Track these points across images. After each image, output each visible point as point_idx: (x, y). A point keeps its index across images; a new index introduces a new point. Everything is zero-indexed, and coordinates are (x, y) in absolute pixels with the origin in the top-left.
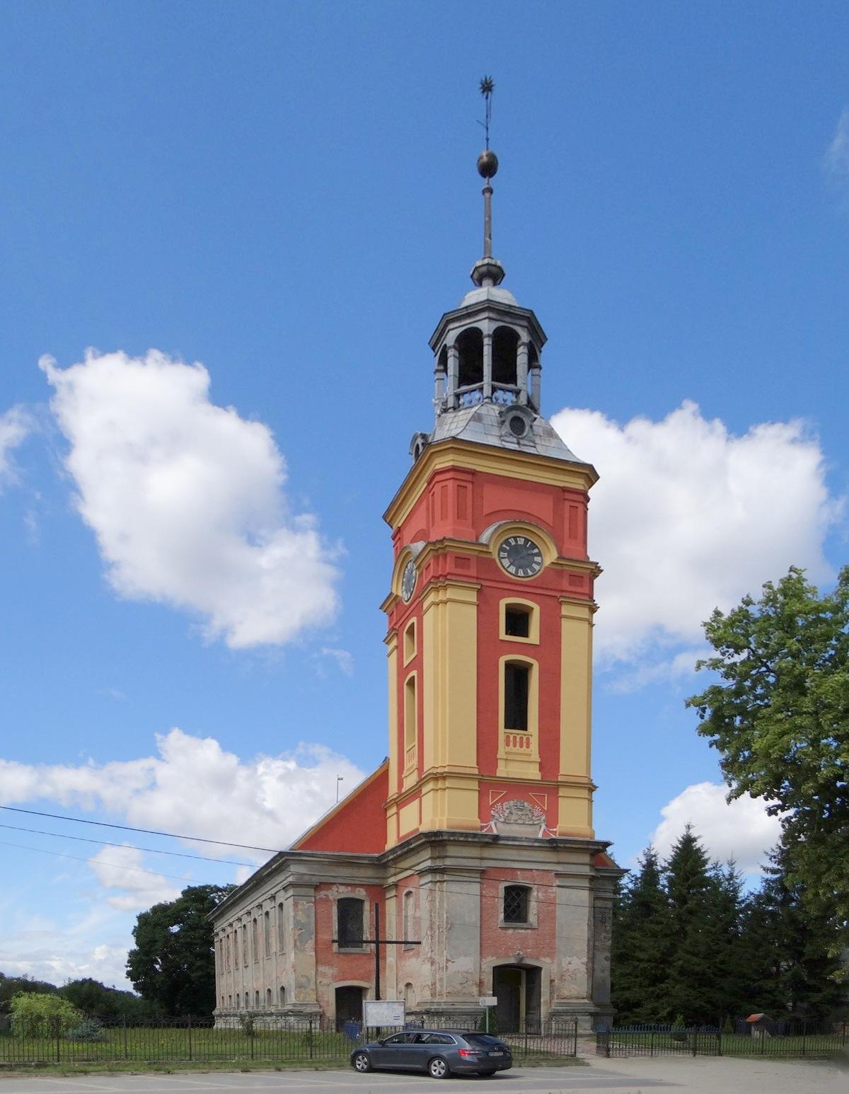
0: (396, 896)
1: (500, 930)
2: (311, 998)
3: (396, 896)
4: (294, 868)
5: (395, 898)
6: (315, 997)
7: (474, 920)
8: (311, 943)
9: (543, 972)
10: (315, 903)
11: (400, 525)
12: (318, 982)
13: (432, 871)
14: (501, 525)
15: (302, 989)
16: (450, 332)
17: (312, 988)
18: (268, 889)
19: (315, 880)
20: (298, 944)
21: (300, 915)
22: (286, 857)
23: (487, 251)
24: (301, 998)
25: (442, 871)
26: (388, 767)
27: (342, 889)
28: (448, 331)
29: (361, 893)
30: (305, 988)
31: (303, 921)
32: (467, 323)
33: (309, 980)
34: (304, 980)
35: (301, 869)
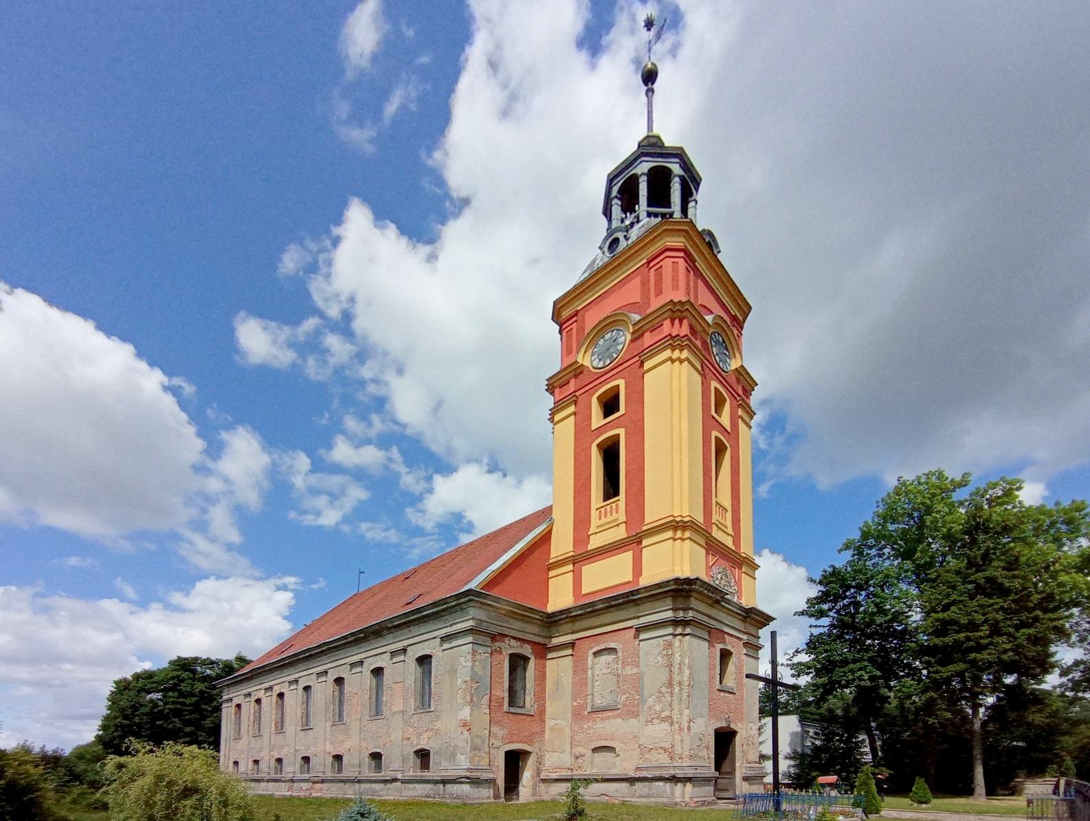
0: (572, 655)
1: (717, 692)
2: (484, 763)
3: (572, 655)
4: (472, 612)
5: (571, 657)
6: (488, 762)
7: (705, 679)
8: (486, 699)
9: (738, 738)
10: (491, 654)
11: (578, 309)
12: (491, 743)
13: (675, 623)
14: (722, 318)
15: (477, 752)
16: (643, 163)
17: (485, 750)
18: (422, 632)
19: (493, 629)
20: (475, 699)
21: (478, 668)
22: (472, 597)
23: (650, 127)
24: (476, 762)
25: (685, 623)
26: (552, 528)
27: (513, 642)
28: (641, 162)
29: (527, 650)
30: (480, 750)
31: (480, 673)
32: (660, 162)
33: (483, 742)
34: (478, 741)
35: (481, 614)
